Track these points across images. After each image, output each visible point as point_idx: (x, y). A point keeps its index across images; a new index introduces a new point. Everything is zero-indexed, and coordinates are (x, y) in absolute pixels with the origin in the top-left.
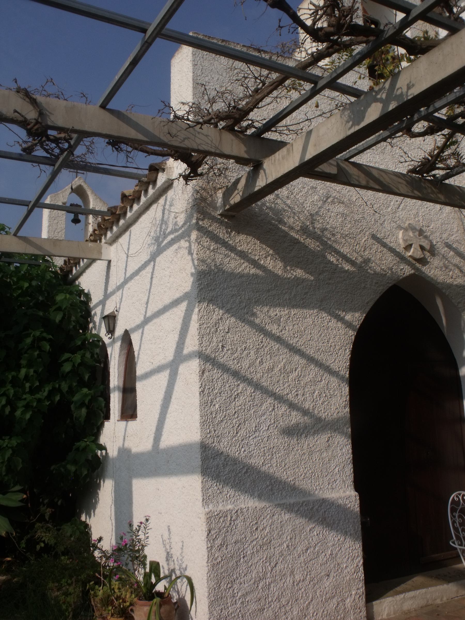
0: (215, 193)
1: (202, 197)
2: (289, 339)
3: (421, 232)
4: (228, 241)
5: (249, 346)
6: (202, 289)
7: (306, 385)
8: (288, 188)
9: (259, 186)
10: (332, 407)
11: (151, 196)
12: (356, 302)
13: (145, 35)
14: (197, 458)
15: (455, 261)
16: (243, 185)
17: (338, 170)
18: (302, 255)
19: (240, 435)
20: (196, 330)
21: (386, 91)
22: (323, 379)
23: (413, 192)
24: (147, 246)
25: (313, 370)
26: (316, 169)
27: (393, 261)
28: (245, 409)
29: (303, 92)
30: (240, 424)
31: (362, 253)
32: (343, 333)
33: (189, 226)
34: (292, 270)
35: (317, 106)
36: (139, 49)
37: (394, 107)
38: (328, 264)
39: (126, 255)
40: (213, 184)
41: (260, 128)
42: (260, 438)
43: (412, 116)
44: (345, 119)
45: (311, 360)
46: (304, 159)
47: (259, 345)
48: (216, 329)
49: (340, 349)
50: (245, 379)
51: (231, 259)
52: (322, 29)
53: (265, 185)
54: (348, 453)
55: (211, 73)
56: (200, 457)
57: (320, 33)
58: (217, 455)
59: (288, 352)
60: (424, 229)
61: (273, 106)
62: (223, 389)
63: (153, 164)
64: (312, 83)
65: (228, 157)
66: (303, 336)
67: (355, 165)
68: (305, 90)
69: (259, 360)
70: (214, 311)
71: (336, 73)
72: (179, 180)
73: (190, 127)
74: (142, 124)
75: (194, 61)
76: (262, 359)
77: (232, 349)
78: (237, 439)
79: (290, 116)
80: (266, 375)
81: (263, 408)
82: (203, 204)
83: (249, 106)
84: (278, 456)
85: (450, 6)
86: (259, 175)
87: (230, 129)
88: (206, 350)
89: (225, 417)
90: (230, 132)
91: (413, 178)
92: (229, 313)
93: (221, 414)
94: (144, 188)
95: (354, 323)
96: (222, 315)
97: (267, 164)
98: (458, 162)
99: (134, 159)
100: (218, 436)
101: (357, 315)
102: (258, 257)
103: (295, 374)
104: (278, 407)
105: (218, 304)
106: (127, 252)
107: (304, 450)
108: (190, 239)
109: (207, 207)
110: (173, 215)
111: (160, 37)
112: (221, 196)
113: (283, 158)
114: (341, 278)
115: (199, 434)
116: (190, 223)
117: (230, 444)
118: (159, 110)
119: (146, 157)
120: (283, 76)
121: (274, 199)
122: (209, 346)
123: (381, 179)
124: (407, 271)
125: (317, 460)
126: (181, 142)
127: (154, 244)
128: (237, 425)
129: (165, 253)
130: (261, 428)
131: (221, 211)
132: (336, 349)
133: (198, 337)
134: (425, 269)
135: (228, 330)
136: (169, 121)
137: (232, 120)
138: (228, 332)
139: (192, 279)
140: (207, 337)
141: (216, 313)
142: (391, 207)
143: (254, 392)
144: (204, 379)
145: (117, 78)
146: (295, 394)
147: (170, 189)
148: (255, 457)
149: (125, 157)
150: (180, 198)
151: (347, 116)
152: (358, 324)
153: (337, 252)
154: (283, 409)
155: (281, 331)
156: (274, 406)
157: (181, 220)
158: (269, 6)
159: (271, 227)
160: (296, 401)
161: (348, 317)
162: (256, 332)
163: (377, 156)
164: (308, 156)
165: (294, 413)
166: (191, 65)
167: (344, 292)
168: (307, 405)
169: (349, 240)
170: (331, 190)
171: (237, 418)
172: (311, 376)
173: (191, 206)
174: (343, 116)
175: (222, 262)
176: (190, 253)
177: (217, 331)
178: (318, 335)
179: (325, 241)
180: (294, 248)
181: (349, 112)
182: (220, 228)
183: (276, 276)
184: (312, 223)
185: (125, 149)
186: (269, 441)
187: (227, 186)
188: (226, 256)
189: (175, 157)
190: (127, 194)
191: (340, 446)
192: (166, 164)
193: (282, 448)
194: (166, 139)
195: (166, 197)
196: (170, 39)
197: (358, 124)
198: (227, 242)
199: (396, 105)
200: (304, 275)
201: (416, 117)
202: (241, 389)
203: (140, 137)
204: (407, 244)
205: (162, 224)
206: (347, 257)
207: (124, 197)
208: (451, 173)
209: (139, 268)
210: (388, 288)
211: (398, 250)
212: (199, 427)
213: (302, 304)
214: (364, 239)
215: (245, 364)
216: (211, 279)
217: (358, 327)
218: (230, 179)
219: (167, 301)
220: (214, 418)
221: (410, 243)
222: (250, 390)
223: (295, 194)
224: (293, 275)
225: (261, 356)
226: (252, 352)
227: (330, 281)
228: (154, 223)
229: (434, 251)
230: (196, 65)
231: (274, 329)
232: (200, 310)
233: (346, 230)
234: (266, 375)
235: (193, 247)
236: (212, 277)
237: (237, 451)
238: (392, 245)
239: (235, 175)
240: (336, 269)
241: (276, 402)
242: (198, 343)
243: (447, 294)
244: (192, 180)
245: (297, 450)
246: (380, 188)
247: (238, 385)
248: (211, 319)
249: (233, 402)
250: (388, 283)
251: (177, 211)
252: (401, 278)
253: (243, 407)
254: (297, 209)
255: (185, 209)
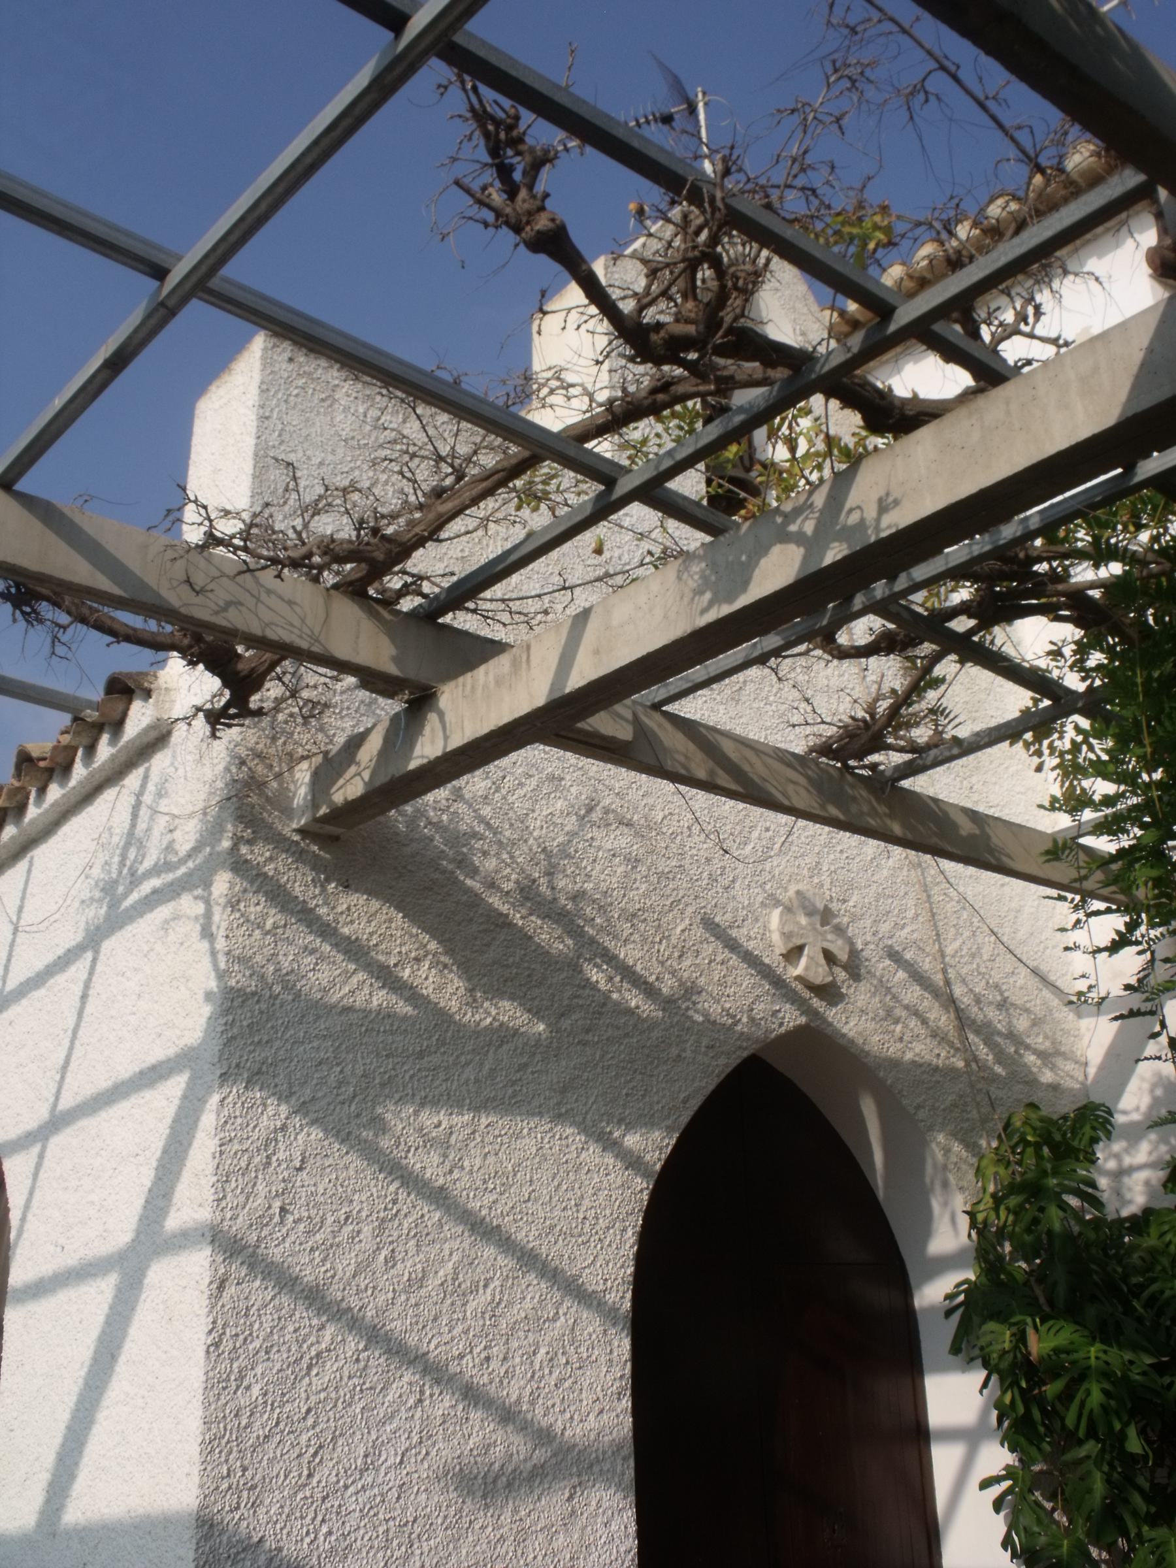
0: (291, 769)
1: (252, 778)
2: (472, 1195)
3: (826, 916)
4: (317, 906)
5: (359, 1212)
6: (233, 1038)
7: (513, 1329)
8: (488, 773)
9: (422, 757)
10: (584, 1395)
11: (103, 765)
12: (656, 1099)
13: (162, 286)
14: (181, 1558)
15: (909, 995)
16: (375, 753)
17: (635, 733)
18: (517, 959)
19: (319, 1482)
20: (209, 1156)
21: (817, 515)
22: (561, 1312)
23: (823, 807)
24: (76, 904)
25: (533, 1289)
26: (579, 725)
27: (753, 988)
28: (337, 1400)
29: (562, 511)
30: (321, 1447)
31: (675, 964)
32: (619, 1182)
33: (210, 855)
34: (487, 999)
35: (599, 551)
36: (138, 322)
37: (839, 557)
38: (584, 987)
39: (11, 927)
40: (285, 743)
41: (437, 596)
42: (376, 1491)
43: (849, 599)
44: (692, 584)
45: (528, 1259)
46: (565, 686)
47: (385, 1209)
48: (268, 1157)
49: (608, 1228)
50: (337, 1313)
51: (322, 958)
52: (659, 326)
53: (439, 753)
54: (626, 1536)
55: (305, 445)
56: (191, 1555)
57: (654, 337)
58: (244, 1550)
59: (466, 1234)
60: (834, 906)
61: (462, 551)
62: (276, 1337)
63: (120, 674)
64: (600, 482)
65: (342, 667)
66: (511, 1186)
67: (675, 720)
68: (567, 505)
69: (384, 1253)
70: (265, 1105)
71: (673, 458)
72: (189, 724)
73: (249, 570)
74: (111, 548)
75: (262, 407)
76: (393, 1251)
77: (309, 1217)
78: (308, 1494)
79: (504, 582)
80: (403, 1297)
81: (390, 1398)
82: (254, 799)
83: (417, 530)
84: (426, 1549)
85: (975, 321)
86: (422, 726)
87: (355, 590)
88: (234, 1218)
89: (277, 1424)
90: (353, 600)
91: (823, 771)
92: (306, 1115)
93: (266, 1416)
94: (86, 741)
95: (648, 1157)
96: (287, 1118)
97: (449, 696)
98: (938, 733)
99: (74, 647)
100: (253, 1488)
101: (657, 1134)
102: (398, 958)
103: (484, 1297)
104: (431, 1395)
105: (276, 1086)
106: (14, 919)
107: (502, 1526)
108: (210, 894)
109: (263, 808)
110: (162, 821)
111: (201, 299)
112: (307, 779)
113: (499, 682)
114: (618, 1028)
115: (196, 1480)
116: (213, 847)
117: (286, 1510)
118: (169, 511)
119: (108, 645)
120: (527, 454)
121: (448, 800)
122: (244, 1208)
123: (746, 767)
124: (791, 1018)
125: (540, 1558)
126: (216, 613)
127: (100, 901)
128: (312, 1450)
129: (129, 928)
130: (383, 1458)
131: (303, 822)
132: (598, 1228)
133: (215, 1179)
134: (833, 1015)
135: (302, 1161)
136: (189, 548)
137: (363, 565)
138: (300, 1169)
139: (207, 1010)
140: (240, 1181)
141: (271, 1111)
142: (752, 845)
143: (366, 1349)
144: (223, 1306)
145: (58, 403)
146: (483, 1356)
147: (160, 750)
148: (360, 1550)
149: (49, 640)
150: (189, 775)
151: (696, 577)
152: (659, 1159)
153: (610, 958)
154: (448, 1400)
155: (451, 1172)
156: (422, 1392)
157: (187, 836)
158: (522, 247)
159: (437, 876)
160: (486, 1376)
161: (632, 1141)
162: (380, 1171)
163: (722, 707)
164: (577, 680)
165: (476, 1415)
166: (254, 417)
167: (623, 1068)
168: (514, 1391)
169: (642, 926)
170: (601, 787)
171: (314, 1427)
172: (527, 1304)
173: (218, 798)
174: (685, 576)
175: (295, 966)
176: (207, 933)
177: (269, 1164)
178: (552, 1188)
179: (579, 926)
180: (494, 939)
181: (703, 565)
182: (297, 869)
183: (441, 1017)
184: (549, 874)
185: (49, 616)
186: (402, 1501)
187: (326, 753)
188: (309, 950)
189: (192, 655)
190: (35, 754)
191: (604, 1513)
192: (156, 677)
193: (440, 1521)
194: (176, 597)
195: (148, 770)
196: (230, 307)
197: (730, 600)
198: (314, 909)
199: (846, 552)
200: (518, 1014)
201: (859, 601)
202: (328, 1338)
203: (103, 583)
204: (791, 945)
205: (128, 845)
206: (634, 973)
207: (25, 761)
208: (920, 762)
209: (47, 966)
210: (738, 1061)
211: (767, 961)
212: (197, 1459)
213: (510, 1098)
214: (680, 926)
215: (345, 1263)
216: (261, 1012)
217: (658, 1167)
218: (334, 735)
219: (126, 1068)
220: (246, 1428)
221: (799, 942)
222: (353, 1344)
223: (504, 792)
224: (489, 1014)
225: (391, 1243)
226: (367, 1230)
227: (589, 1037)
228: (103, 840)
229: (858, 967)
230: (267, 418)
231: (427, 1163)
232: (224, 1098)
233: (636, 897)
234: (403, 1297)
235: (216, 918)
236: (263, 1006)
237: (308, 1533)
238: (751, 945)
239: (348, 724)
240: (604, 1004)
241: (427, 1378)
242: (212, 1198)
243: (889, 1082)
244: (229, 726)
245: (483, 1528)
246: (740, 789)
247: (322, 1327)
248: (255, 1127)
249: (303, 1378)
250: (740, 1047)
251: (176, 812)
252: (773, 1035)
253: (333, 1395)
254: (507, 834)
255: (200, 805)
